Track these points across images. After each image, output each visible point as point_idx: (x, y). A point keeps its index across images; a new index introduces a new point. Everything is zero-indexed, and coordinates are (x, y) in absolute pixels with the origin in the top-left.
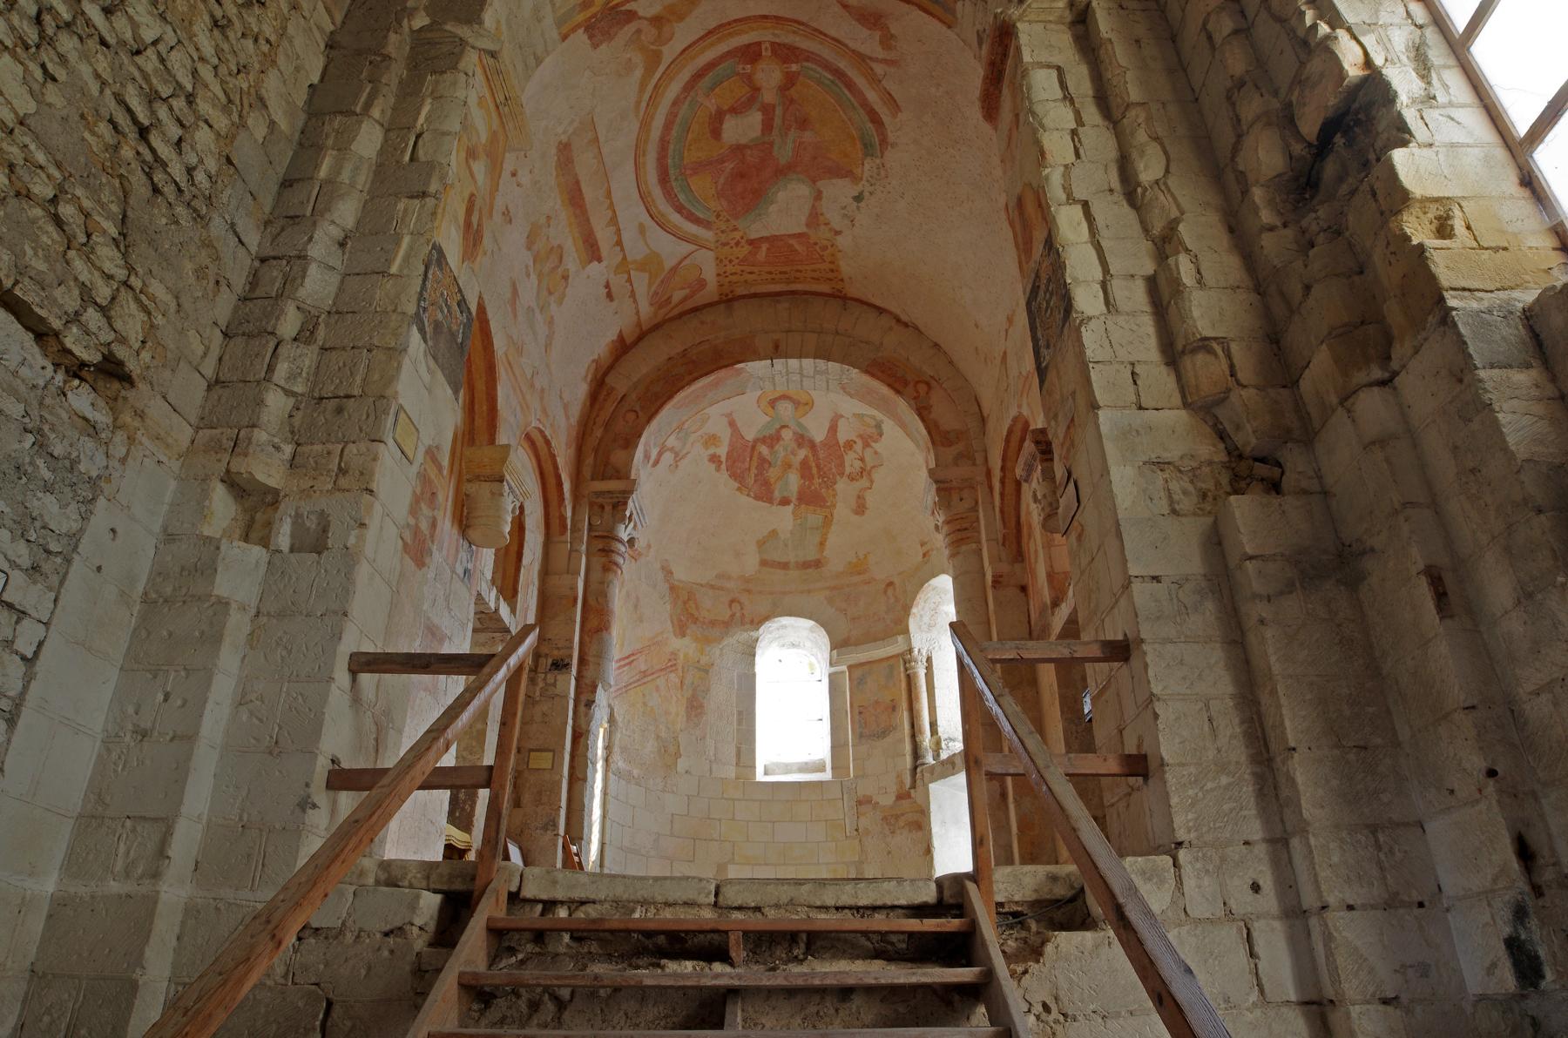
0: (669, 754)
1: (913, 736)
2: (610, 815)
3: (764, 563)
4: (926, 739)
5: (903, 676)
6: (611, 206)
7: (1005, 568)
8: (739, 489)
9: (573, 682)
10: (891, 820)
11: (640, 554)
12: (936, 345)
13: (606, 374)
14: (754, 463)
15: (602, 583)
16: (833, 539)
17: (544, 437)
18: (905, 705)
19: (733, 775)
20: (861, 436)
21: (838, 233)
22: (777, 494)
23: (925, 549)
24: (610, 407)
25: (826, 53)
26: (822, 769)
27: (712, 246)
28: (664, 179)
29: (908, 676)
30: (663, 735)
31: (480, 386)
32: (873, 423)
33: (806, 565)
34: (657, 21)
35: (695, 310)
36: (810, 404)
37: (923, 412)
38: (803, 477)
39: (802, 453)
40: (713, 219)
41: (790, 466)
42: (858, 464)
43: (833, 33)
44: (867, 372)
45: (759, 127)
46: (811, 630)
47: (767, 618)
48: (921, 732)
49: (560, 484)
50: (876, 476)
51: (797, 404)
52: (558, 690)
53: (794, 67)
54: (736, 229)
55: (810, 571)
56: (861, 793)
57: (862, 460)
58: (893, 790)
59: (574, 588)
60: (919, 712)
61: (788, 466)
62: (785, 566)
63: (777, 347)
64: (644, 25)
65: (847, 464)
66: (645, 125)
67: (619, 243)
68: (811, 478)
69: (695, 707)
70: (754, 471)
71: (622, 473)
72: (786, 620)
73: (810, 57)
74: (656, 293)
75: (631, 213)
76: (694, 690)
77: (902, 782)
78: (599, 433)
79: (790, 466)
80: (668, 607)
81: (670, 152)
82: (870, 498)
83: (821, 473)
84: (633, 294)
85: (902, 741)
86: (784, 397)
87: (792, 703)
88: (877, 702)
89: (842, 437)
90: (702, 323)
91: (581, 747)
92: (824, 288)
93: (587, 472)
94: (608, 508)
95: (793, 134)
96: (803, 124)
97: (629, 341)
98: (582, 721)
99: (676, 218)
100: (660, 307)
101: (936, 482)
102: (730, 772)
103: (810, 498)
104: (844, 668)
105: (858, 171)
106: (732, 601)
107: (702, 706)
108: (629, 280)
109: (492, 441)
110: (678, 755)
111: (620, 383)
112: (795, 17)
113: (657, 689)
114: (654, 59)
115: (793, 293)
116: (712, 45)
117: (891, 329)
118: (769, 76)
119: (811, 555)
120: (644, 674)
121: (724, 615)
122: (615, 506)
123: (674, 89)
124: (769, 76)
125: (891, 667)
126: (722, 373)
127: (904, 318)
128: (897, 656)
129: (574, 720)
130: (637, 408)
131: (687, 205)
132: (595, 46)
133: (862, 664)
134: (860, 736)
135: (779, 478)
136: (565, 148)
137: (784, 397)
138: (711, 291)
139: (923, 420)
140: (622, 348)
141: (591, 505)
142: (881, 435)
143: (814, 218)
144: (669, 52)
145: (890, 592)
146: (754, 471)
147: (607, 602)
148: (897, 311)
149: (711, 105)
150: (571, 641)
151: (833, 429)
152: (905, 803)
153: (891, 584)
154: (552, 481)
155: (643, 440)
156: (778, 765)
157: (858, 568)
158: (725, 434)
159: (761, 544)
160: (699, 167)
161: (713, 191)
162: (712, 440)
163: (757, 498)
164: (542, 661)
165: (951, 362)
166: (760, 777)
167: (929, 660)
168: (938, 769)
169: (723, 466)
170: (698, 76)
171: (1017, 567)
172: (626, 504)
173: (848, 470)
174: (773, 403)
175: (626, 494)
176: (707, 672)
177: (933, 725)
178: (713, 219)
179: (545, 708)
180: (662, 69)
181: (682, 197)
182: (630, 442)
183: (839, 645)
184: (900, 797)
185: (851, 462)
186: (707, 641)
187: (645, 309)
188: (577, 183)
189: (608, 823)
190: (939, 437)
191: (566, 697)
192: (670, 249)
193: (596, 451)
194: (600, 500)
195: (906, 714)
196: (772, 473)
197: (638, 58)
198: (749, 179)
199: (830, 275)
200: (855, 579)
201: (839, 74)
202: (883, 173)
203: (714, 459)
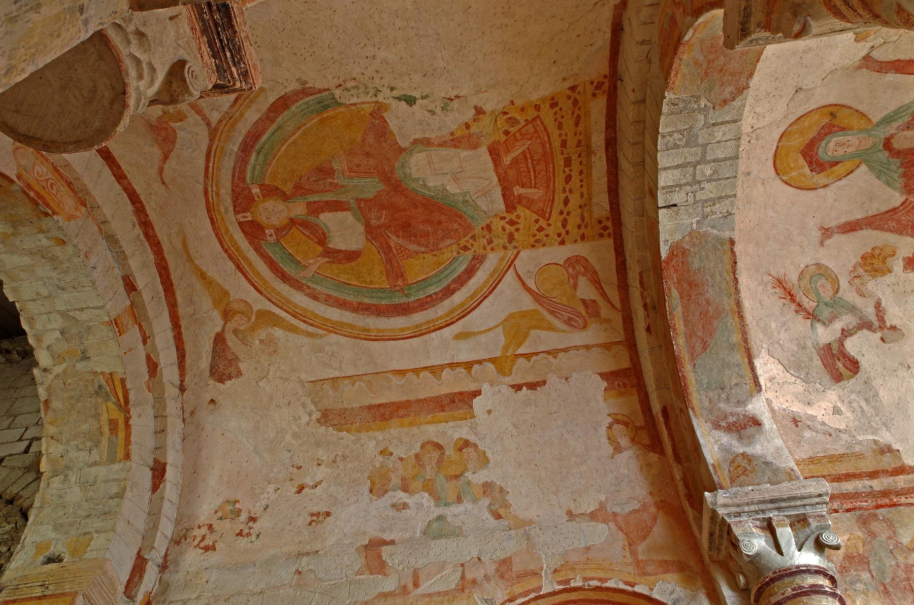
6: (416, 371)
21: (479, 111)
25: (228, 165)
27: (510, 253)
28: (405, 310)
34: (227, 315)
40: (469, 255)
43: (201, 162)
45: (340, 215)
51: (828, 130)
53: (256, 190)
54: (489, 228)
64: (230, 326)
66: (335, 328)
67: (468, 365)
73: (239, 174)
74: (569, 322)
75: (440, 347)
81: (371, 301)
84: (554, 353)
92: (597, 108)
95: (339, 180)
96: (325, 171)
97: (625, 363)
99: (459, 297)
100: (596, 314)
105: (368, 108)
108: (528, 356)
112: (202, 195)
114: (263, 315)
116: (250, 264)
118: (272, 212)
123: (300, 299)
124: (272, 212)
131: (444, 284)
132: (239, 374)
136: (326, 417)
143: (462, 140)
144: (259, 303)
149: (316, 263)
158: (871, 238)
160: (395, 273)
161: (429, 257)
170: (284, 277)
178: (469, 255)
180: (277, 311)
181: (432, 290)
187: (592, 335)
188: (370, 408)
192: (509, 299)
197: (262, 333)
198: (410, 219)
201: (247, 147)
202: (350, 84)
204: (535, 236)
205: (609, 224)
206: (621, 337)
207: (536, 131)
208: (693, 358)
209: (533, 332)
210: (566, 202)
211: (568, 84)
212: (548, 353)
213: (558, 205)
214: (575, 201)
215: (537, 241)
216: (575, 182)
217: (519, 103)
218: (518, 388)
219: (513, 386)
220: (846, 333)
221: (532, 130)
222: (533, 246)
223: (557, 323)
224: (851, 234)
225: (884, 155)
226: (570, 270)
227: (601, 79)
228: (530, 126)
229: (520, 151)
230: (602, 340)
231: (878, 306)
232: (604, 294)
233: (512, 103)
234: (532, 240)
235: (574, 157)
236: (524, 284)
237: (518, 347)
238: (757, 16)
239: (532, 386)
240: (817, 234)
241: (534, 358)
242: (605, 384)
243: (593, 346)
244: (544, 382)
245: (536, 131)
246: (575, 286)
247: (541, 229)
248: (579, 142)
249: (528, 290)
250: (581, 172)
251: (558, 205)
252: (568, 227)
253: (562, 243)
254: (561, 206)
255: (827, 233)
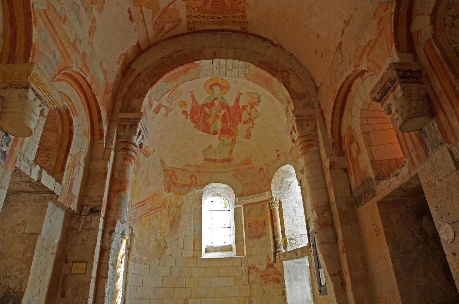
0: (161, 248)
1: (274, 238)
2: (129, 283)
3: (206, 160)
4: (280, 240)
5: (268, 210)
7: (336, 159)
8: (195, 127)
9: (102, 221)
10: (264, 277)
11: (149, 154)
12: (291, 54)
13: (131, 63)
14: (202, 116)
15: (123, 166)
16: (235, 149)
17: (87, 82)
18: (270, 223)
19: (192, 255)
20: (250, 103)
22: (212, 130)
23: (278, 153)
24: (132, 78)
26: (231, 250)
29: (271, 210)
30: (159, 238)
31: (21, 26)
32: (256, 96)
33: (223, 161)
35: (176, 36)
36: (228, 88)
37: (286, 85)
38: (223, 122)
39: (223, 111)
41: (218, 117)
42: (248, 116)
44: (258, 66)
46: (226, 189)
47: (207, 184)
48: (278, 236)
49: (99, 112)
50: (255, 121)
51: (222, 88)
52: (93, 226)
55: (225, 163)
56: (250, 263)
57: (250, 114)
58: (265, 263)
59: (105, 168)
60: (277, 227)
61: (217, 117)
62: (215, 161)
63: (215, 54)
65: (243, 116)
68: (227, 123)
69: (174, 224)
70: (202, 119)
71: (137, 110)
72: (215, 185)
74: (156, 23)
76: (174, 216)
77: (269, 260)
78: (125, 90)
79: (218, 117)
80: (163, 178)
82: (252, 131)
83: (232, 119)
84: (144, 21)
85: (269, 240)
86: (216, 84)
87: (217, 221)
88: (257, 222)
89: (241, 104)
90: (179, 42)
91: (105, 257)
93: (118, 108)
94: (128, 127)
97: (143, 48)
98: (107, 243)
100: (159, 32)
101: (296, 116)
102: (191, 254)
103: (226, 132)
104: (241, 206)
106: (192, 176)
107: (177, 224)
108: (141, 11)
109: (26, 60)
110: (166, 247)
111: (138, 67)
113: (156, 216)
115: (223, 30)
117: (269, 47)
119: (226, 156)
120: (150, 210)
121: (188, 183)
122: (131, 126)
125: (263, 206)
126: (188, 65)
127: (276, 42)
128: (265, 201)
129: (102, 242)
130: (146, 80)
133: (249, 204)
134: (249, 237)
135: (213, 123)
137: (216, 84)
138: (183, 27)
139: (286, 87)
140: (139, 51)
141: (119, 126)
142: (259, 102)
145: (261, 172)
146: (202, 119)
147: (125, 176)
148: (272, 38)
150: (102, 197)
151: (238, 100)
152: (271, 270)
153: (262, 169)
154: (94, 110)
155: (148, 95)
156: (211, 247)
157: (247, 162)
158: (190, 101)
159: (204, 151)
162: (183, 104)
163: (203, 131)
164: (85, 208)
165: (298, 62)
166: (206, 256)
167: (280, 203)
168: (288, 255)
169: (189, 116)
171: (342, 158)
172: (137, 125)
173: (243, 119)
174: (211, 87)
175: (137, 120)
176: (180, 208)
177: (283, 232)
179: (84, 236)
182: (141, 96)
183: (239, 195)
184: (268, 266)
185: (245, 115)
186: (180, 194)
187: (151, 32)
189: (128, 288)
190: (295, 96)
191: (96, 230)
193: (123, 99)
194: (124, 123)
195: (270, 227)
196: (210, 120)
199: (241, 20)
200: (246, 167)
203: (184, 113)
204: (191, 7)
205: (193, 31)
206: (151, 43)
207: (233, 9)
208: (164, 80)
209: (151, 11)
210: (203, 17)
211: (249, 22)
212: (144, 19)
213: (202, 14)
214: (204, 19)
215: (189, 8)
216: (212, 20)
217: (247, 7)
218: (129, 12)
219: (129, 9)
220: (165, 106)
221: (234, 8)
222: (187, 6)
223: (155, 19)
224: (191, 97)
225: (213, 98)
226: (176, 20)
227: (247, 30)
228: (236, 8)
229: (227, 3)
230: (150, 37)
231: (172, 109)
232: (166, 33)
233: (247, 5)
234: (190, 6)
235: (220, 20)
236: (171, 4)
237: (145, 6)
238: (299, 118)
239: (131, 17)
240: (191, 90)
241: (141, 14)
242: (135, 44)
243: (148, 35)
244: (133, 22)
245: (233, 9)
246: (169, 23)
247: (194, 9)
248: (226, 22)
249: (169, 6)
250: (214, 22)
251: (202, 14)
252: (193, 18)
253: (187, 16)
254: (202, 15)
255: (191, 92)
